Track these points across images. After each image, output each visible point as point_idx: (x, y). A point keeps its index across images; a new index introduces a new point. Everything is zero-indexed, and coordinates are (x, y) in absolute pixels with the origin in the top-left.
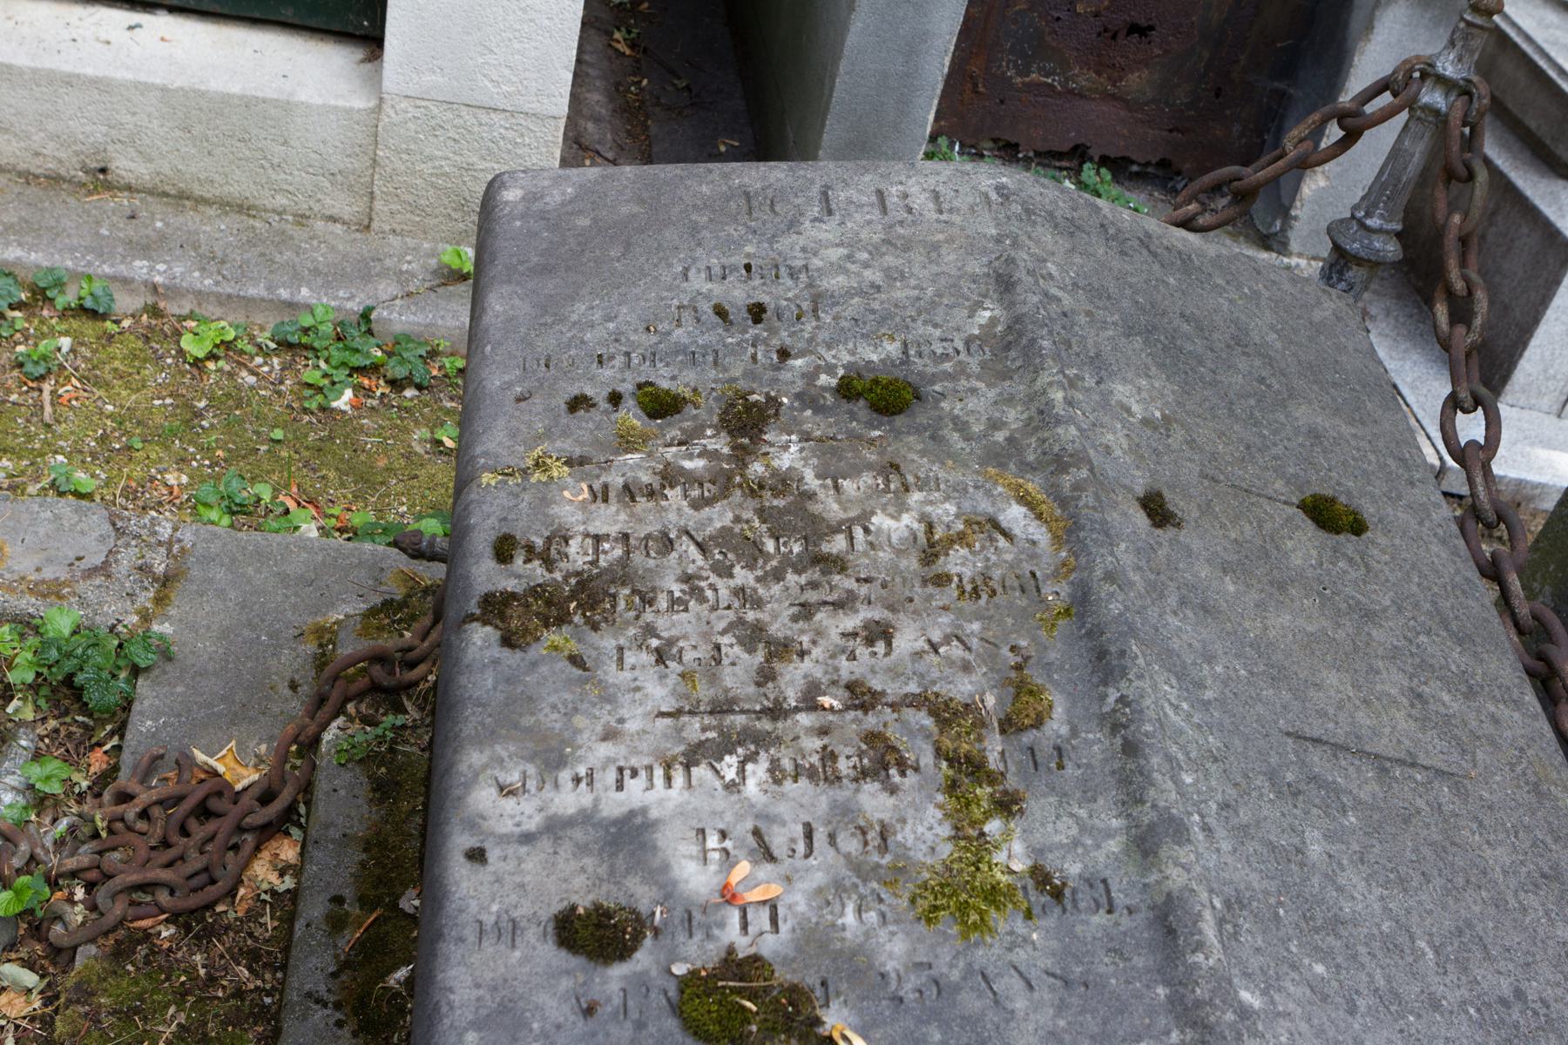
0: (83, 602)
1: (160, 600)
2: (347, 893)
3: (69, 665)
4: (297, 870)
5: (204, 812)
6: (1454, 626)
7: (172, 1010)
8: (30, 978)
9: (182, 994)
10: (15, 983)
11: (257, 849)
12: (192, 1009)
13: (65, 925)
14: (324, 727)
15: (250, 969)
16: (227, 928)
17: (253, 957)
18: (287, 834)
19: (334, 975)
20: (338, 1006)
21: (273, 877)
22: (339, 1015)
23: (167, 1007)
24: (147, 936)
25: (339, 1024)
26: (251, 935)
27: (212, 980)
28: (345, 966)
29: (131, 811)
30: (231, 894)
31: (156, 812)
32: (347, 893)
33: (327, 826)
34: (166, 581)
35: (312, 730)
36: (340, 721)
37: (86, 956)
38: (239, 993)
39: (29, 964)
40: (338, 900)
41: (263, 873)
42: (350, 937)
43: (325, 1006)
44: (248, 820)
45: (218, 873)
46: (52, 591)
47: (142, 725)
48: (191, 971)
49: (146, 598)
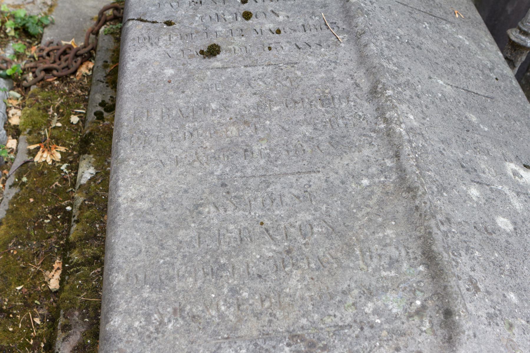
0: (27, 9)
1: (50, 11)
2: (109, 60)
3: (24, 22)
4: (92, 70)
5: (65, 53)
6: (205, 270)
7: (59, 99)
8: (18, 95)
9: (61, 96)
10: (14, 96)
11: (82, 64)
12: (65, 98)
13: (27, 81)
14: (100, 28)
15: (81, 91)
16: (74, 82)
17: (82, 88)
18: (91, 61)
19: (105, 77)
20: (107, 83)
21: (87, 71)
22: (107, 84)
23: (58, 98)
24: (50, 83)
25: (107, 86)
26: (81, 83)
27: (70, 93)
28: (108, 75)
29: (44, 53)
30: (74, 73)
31: (51, 53)
32: (109, 60)
33: (102, 47)
34: (51, 6)
35: (96, 28)
36: (105, 26)
37: (33, 88)
38: (78, 95)
39: (18, 92)
40: (106, 62)
41: (83, 70)
42: (108, 70)
43: (103, 82)
44: (79, 52)
45: (70, 66)
46: (18, 6)
47: (46, 39)
48: (64, 91)
49: (46, 10)
